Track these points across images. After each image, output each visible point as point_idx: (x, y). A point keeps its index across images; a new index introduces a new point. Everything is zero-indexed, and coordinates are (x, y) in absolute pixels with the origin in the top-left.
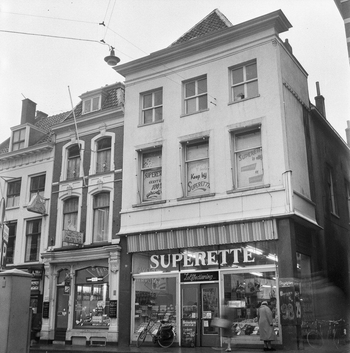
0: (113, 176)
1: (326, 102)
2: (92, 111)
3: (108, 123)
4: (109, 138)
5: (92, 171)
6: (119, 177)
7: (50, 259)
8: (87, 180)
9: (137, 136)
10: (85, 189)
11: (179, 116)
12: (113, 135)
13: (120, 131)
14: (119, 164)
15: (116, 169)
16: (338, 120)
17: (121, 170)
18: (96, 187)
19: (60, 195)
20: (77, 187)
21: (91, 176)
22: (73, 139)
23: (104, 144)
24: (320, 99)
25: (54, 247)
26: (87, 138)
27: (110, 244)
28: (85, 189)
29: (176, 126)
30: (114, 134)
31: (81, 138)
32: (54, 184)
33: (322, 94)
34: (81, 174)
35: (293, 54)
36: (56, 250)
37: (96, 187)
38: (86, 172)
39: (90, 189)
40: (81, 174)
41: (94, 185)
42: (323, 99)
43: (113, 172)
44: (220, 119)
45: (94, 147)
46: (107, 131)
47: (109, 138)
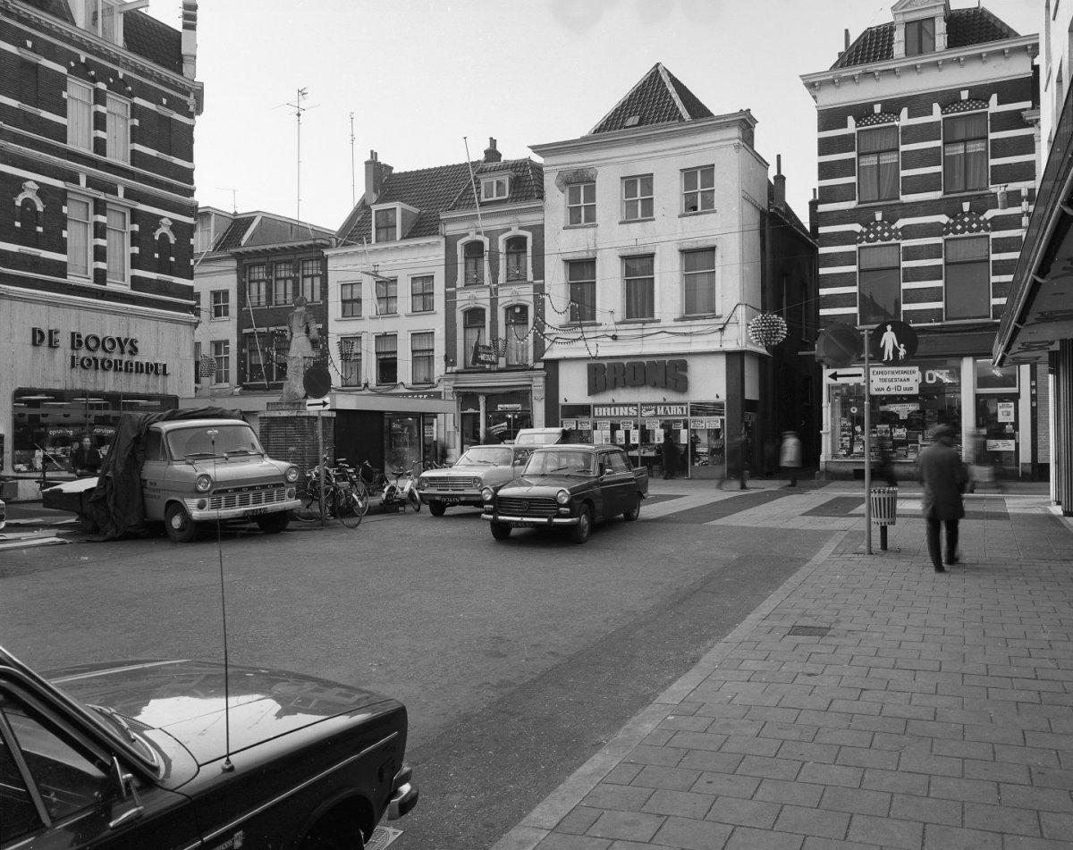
0: (531, 286)
1: (786, 181)
2: (495, 198)
3: (522, 218)
4: (524, 239)
5: (502, 278)
6: (539, 290)
7: (452, 382)
8: (496, 289)
9: (562, 242)
10: (494, 302)
11: (617, 222)
12: (529, 235)
13: (538, 231)
14: (539, 272)
15: (535, 279)
16: (799, 201)
17: (542, 281)
18: (508, 299)
19: (459, 304)
20: (482, 298)
21: (502, 285)
22: (471, 234)
23: (516, 244)
24: (780, 179)
25: (455, 369)
26: (492, 235)
27: (532, 369)
28: (494, 302)
29: (610, 238)
30: (531, 233)
31: (487, 234)
32: (448, 290)
33: (783, 173)
34: (487, 280)
35: (755, 149)
36: (458, 372)
37: (510, 299)
38: (495, 281)
39: (500, 301)
40: (487, 280)
41: (506, 297)
42: (784, 178)
43: (532, 282)
44: (667, 233)
45: (502, 247)
46: (520, 228)
47: (524, 239)
